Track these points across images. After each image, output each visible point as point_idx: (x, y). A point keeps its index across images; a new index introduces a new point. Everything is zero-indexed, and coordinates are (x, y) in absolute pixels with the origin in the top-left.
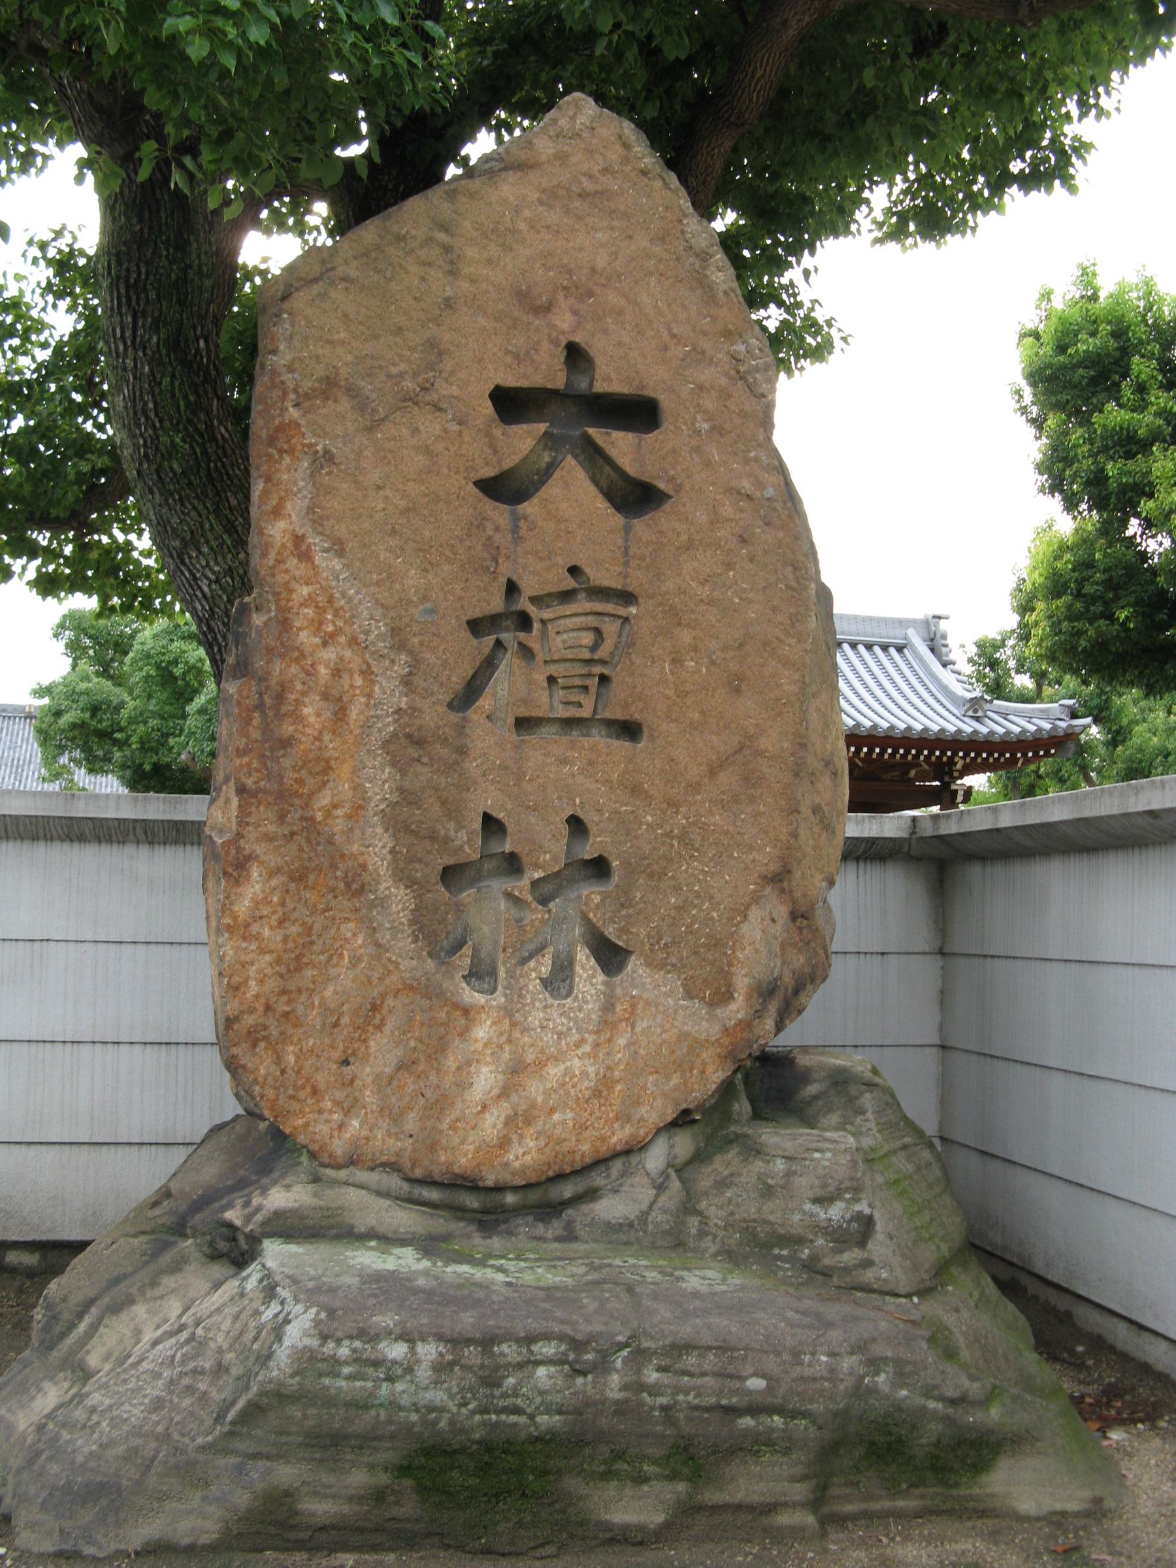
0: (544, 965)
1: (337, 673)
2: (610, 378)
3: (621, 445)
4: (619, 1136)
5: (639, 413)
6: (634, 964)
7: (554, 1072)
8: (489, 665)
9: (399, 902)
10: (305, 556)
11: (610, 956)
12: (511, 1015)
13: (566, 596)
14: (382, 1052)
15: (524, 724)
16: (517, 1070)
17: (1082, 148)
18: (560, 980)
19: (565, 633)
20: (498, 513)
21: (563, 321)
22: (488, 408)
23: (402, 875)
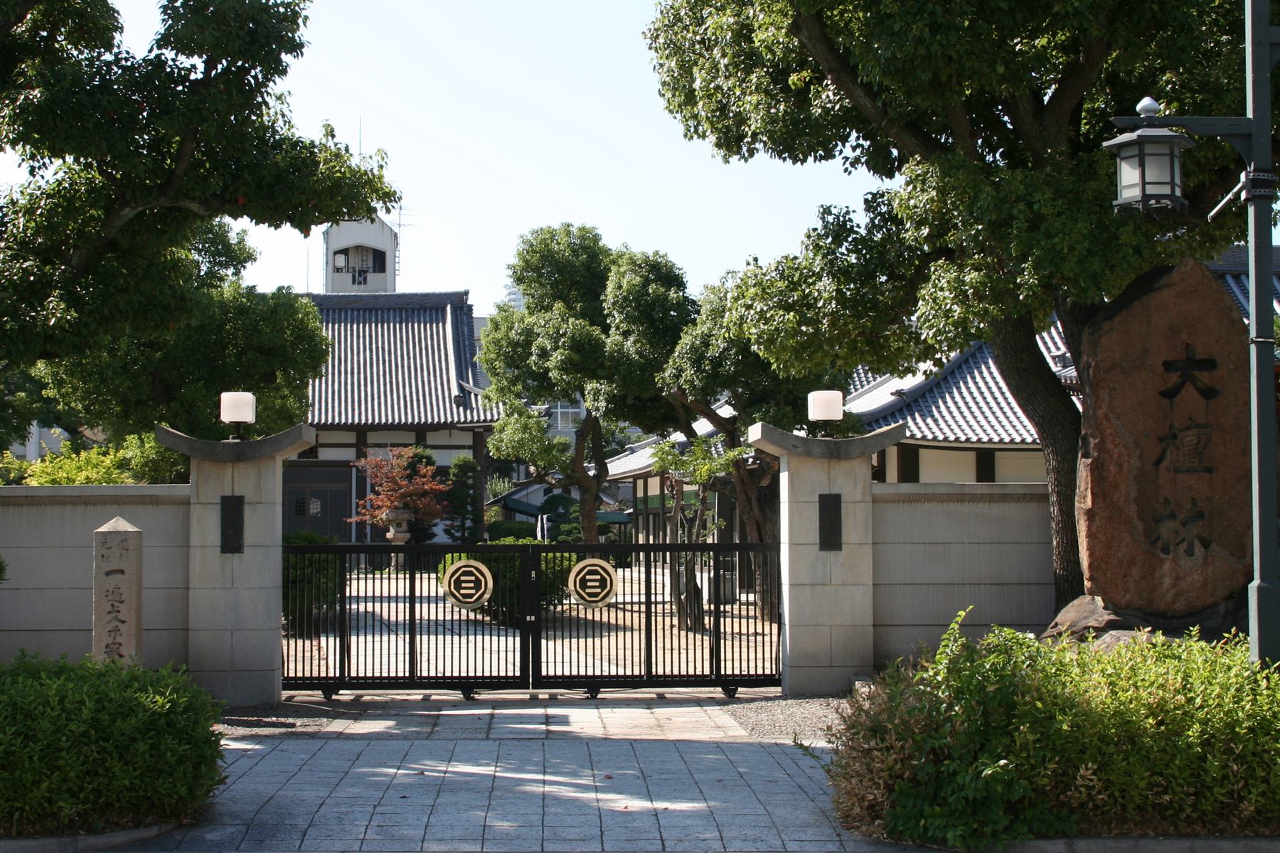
0: (1185, 545)
1: (1119, 456)
2: (1201, 354)
3: (1204, 377)
4: (1210, 600)
5: (1209, 364)
6: (1214, 546)
7: (1189, 579)
8: (1165, 450)
9: (1140, 526)
10: (1109, 420)
11: (1206, 545)
12: (1175, 561)
13: (1188, 428)
14: (1135, 572)
15: (1176, 471)
16: (1178, 578)
17: (306, 232)
18: (1190, 553)
19: (1190, 438)
20: (1166, 401)
21: (1184, 336)
22: (1162, 368)
23: (1140, 518)
